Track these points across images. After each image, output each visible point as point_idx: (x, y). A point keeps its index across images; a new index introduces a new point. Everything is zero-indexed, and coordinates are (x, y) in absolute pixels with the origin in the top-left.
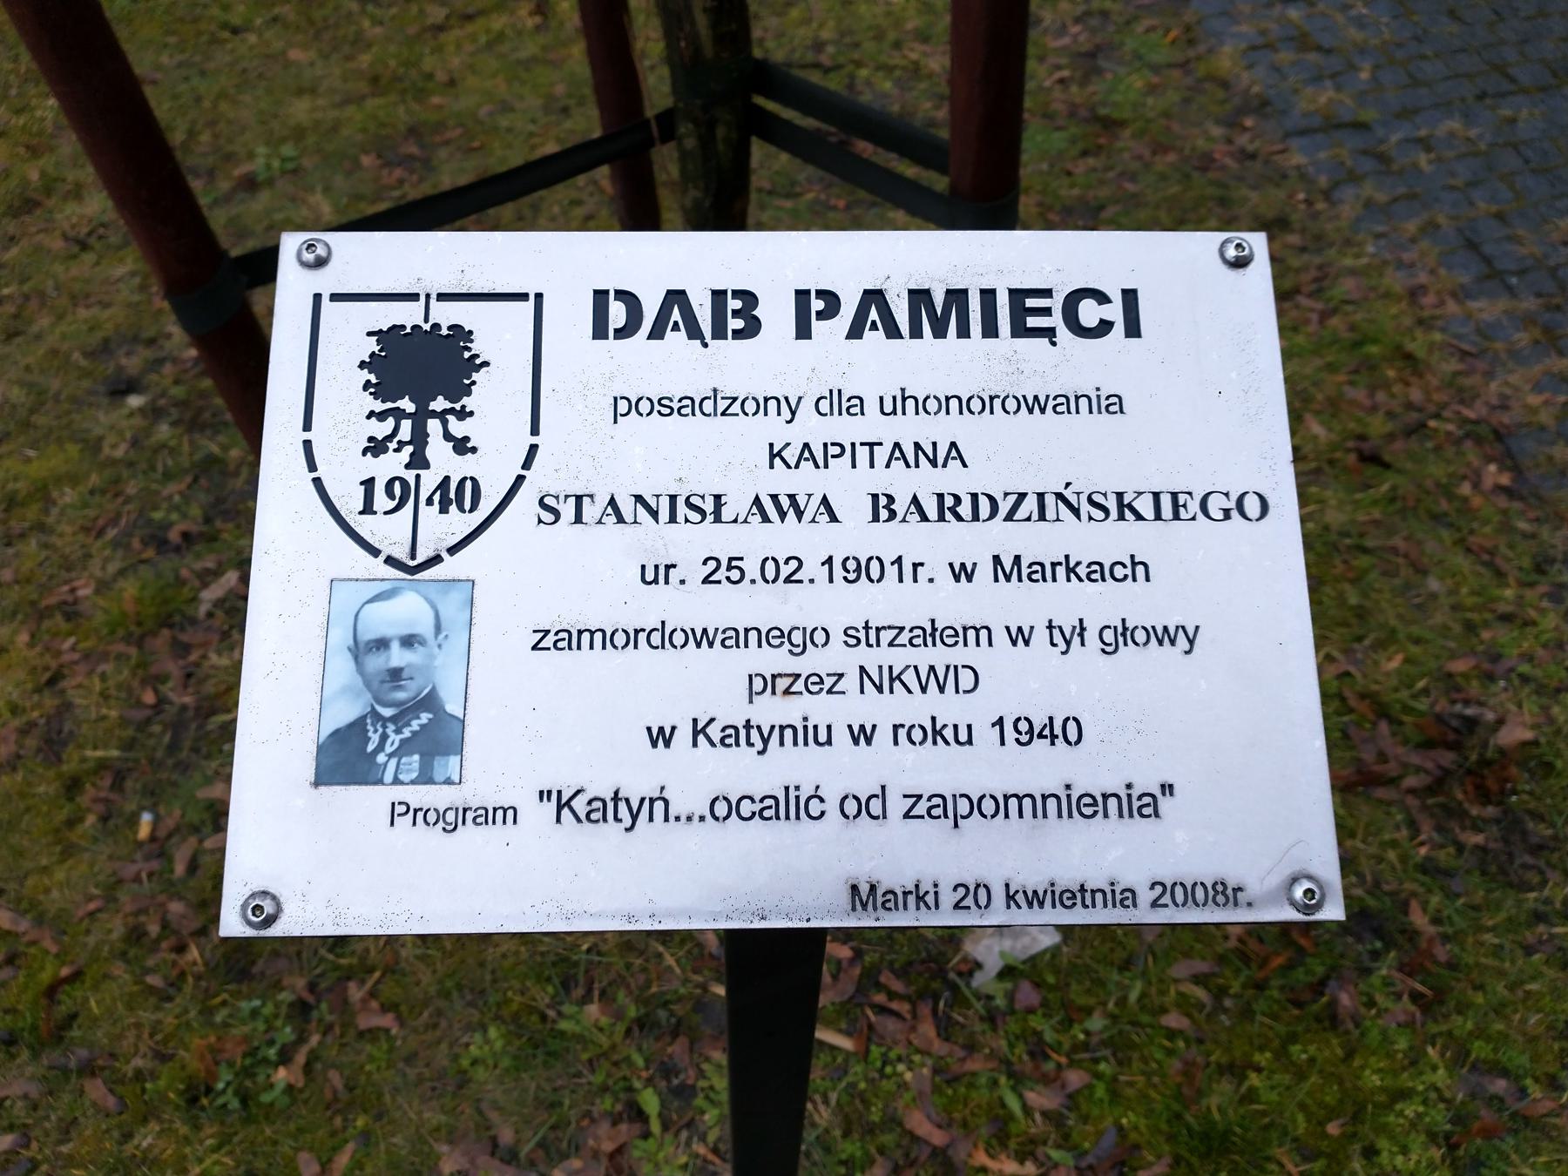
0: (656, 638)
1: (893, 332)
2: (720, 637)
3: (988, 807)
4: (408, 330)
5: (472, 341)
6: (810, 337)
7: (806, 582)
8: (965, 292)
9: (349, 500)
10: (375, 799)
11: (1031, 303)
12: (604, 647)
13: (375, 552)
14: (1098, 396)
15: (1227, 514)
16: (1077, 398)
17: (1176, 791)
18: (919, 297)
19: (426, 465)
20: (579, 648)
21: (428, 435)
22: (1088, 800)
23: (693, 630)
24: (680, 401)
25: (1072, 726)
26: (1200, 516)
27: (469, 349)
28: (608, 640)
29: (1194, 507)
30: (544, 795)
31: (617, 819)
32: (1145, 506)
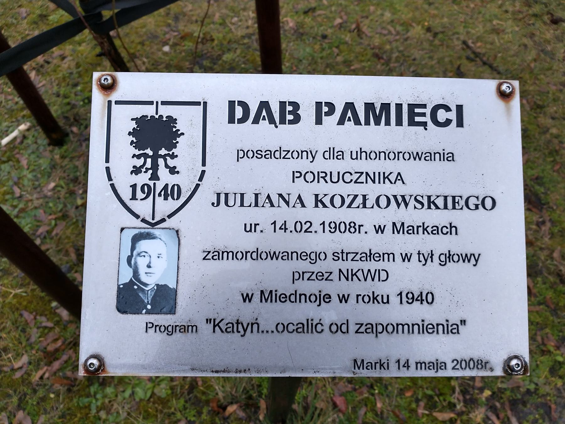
0: (254, 256)
1: (357, 122)
2: (281, 255)
3: (390, 328)
4: (149, 118)
5: (176, 123)
6: (229, 123)
7: (313, 232)
8: (235, 101)
9: (126, 194)
10: (141, 320)
11: (417, 110)
12: (233, 259)
13: (137, 217)
14: (444, 153)
15: (477, 207)
16: (435, 154)
17: (467, 323)
18: (369, 107)
19: (158, 179)
20: (222, 259)
21: (158, 166)
22: (430, 326)
23: (461, 255)
24: (265, 152)
25: (430, 296)
26: (465, 207)
27: (175, 127)
28: (235, 256)
29: (462, 203)
30: (208, 321)
31: (238, 332)
32: (440, 202)
